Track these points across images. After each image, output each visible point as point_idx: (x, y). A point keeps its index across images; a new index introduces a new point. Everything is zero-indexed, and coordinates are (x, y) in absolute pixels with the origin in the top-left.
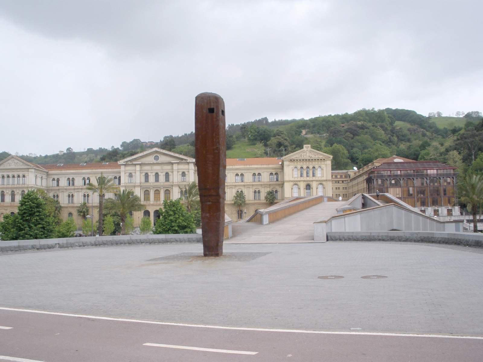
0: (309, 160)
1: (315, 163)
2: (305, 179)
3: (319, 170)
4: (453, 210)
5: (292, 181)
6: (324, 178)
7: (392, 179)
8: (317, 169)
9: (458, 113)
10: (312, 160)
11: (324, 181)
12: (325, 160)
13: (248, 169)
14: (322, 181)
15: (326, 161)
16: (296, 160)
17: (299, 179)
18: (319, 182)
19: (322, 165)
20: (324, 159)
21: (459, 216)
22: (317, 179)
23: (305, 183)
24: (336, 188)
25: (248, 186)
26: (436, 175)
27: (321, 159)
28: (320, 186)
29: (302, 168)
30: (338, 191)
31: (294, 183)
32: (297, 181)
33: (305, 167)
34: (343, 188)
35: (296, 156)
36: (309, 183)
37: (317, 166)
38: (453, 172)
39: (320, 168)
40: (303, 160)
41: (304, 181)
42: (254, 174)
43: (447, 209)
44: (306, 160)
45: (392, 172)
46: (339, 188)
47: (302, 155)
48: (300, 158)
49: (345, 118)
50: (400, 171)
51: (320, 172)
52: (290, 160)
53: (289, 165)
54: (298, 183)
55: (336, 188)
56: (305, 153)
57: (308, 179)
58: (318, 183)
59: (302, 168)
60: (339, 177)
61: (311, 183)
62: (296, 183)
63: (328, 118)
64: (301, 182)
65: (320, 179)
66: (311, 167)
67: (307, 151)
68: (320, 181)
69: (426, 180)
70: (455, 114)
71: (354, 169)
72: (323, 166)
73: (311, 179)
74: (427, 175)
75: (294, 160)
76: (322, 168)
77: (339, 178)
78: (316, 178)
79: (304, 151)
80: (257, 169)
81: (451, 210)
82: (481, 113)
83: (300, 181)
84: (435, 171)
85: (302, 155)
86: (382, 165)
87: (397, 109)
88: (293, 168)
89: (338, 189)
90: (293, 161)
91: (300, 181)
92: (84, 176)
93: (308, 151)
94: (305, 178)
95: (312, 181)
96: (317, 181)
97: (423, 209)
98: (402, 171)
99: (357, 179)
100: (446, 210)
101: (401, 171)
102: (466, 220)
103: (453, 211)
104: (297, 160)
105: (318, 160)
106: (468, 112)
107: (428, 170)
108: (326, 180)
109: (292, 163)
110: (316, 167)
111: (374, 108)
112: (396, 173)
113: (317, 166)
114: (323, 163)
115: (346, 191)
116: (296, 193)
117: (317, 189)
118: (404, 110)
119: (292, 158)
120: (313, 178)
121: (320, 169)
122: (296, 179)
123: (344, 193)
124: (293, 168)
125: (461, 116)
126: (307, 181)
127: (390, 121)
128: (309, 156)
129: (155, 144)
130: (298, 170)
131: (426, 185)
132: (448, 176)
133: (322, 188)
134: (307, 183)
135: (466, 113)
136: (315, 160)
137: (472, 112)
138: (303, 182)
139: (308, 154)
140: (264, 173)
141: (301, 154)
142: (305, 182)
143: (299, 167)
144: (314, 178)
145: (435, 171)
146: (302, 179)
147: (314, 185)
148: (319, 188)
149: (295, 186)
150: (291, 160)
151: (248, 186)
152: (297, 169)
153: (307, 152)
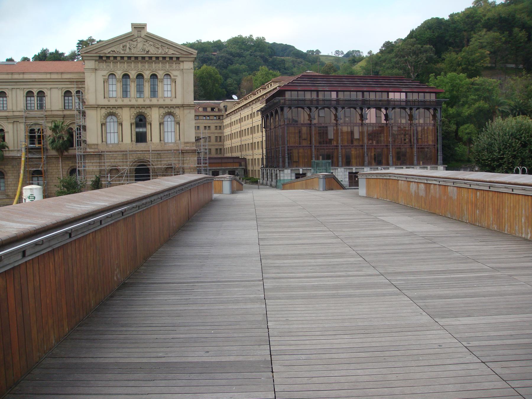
0: (143, 58)
2: (133, 102)
5: (103, 107)
6: (178, 101)
7: (319, 108)
8: (162, 80)
9: (337, 52)
10: (150, 58)
11: (178, 107)
12: (181, 59)
13: (17, 82)
14: (172, 106)
15: (183, 62)
16: (112, 59)
17: (120, 102)
18: (167, 110)
19: (173, 70)
20: (178, 58)
22: (161, 102)
23: (134, 112)
24: (205, 127)
25: (16, 120)
26: (404, 103)
27: (171, 58)
28: (169, 120)
29: (126, 76)
30: (207, 131)
31: (109, 110)
32: (114, 107)
33: (133, 74)
34: (216, 127)
35: (113, 49)
36: (143, 110)
38: (436, 98)
39: (168, 77)
40: (129, 58)
41: (132, 107)
42: (30, 94)
44: (136, 58)
45: (321, 94)
46: (209, 127)
47: (128, 46)
48: (123, 52)
49: (218, 45)
50: (404, 94)
52: (97, 58)
53: (96, 69)
54: (119, 111)
55: (205, 127)
56: (135, 43)
57: (141, 102)
58: (162, 111)
59: (126, 76)
60: (209, 109)
61: (147, 111)
62: (111, 111)
64: (124, 109)
65: (168, 102)
66: (147, 74)
67: (138, 37)
68: (167, 106)
69: (334, 113)
70: (334, 53)
71: (233, 99)
73: (148, 102)
74: (388, 101)
75: (108, 58)
76: (173, 77)
77: (209, 112)
78: (158, 101)
79: (131, 38)
80: (35, 81)
82: (362, 52)
83: (121, 107)
84: (403, 96)
85: (126, 46)
86: (298, 79)
87: (275, 43)
88: (107, 77)
89: (207, 128)
90: (105, 61)
92: (29, 87)
93: (141, 37)
94: (133, 99)
95: (150, 107)
96: (161, 107)
98: (408, 94)
99: (239, 113)
101: (363, 92)
104: (115, 58)
105: (164, 58)
106: (348, 51)
107: (390, 93)
108: (183, 106)
109: (103, 65)
110: (160, 74)
112: (327, 96)
114: (174, 66)
115: (209, 131)
116: (112, 134)
117: (162, 126)
118: (282, 44)
119: (103, 52)
122: (113, 102)
123: (216, 135)
125: (340, 56)
126: (138, 107)
128: (144, 50)
131: (335, 122)
132: (425, 105)
133: (173, 123)
134: (138, 110)
135: (345, 53)
136: (157, 58)
137: (353, 51)
139: (140, 46)
140: (53, 90)
141: (124, 44)
142: (133, 110)
143: (119, 74)
144: (154, 101)
145: (403, 96)
146: (126, 101)
147: (154, 116)
148: (166, 123)
149: (110, 117)
150: (101, 57)
151: (16, 120)
153: (139, 40)
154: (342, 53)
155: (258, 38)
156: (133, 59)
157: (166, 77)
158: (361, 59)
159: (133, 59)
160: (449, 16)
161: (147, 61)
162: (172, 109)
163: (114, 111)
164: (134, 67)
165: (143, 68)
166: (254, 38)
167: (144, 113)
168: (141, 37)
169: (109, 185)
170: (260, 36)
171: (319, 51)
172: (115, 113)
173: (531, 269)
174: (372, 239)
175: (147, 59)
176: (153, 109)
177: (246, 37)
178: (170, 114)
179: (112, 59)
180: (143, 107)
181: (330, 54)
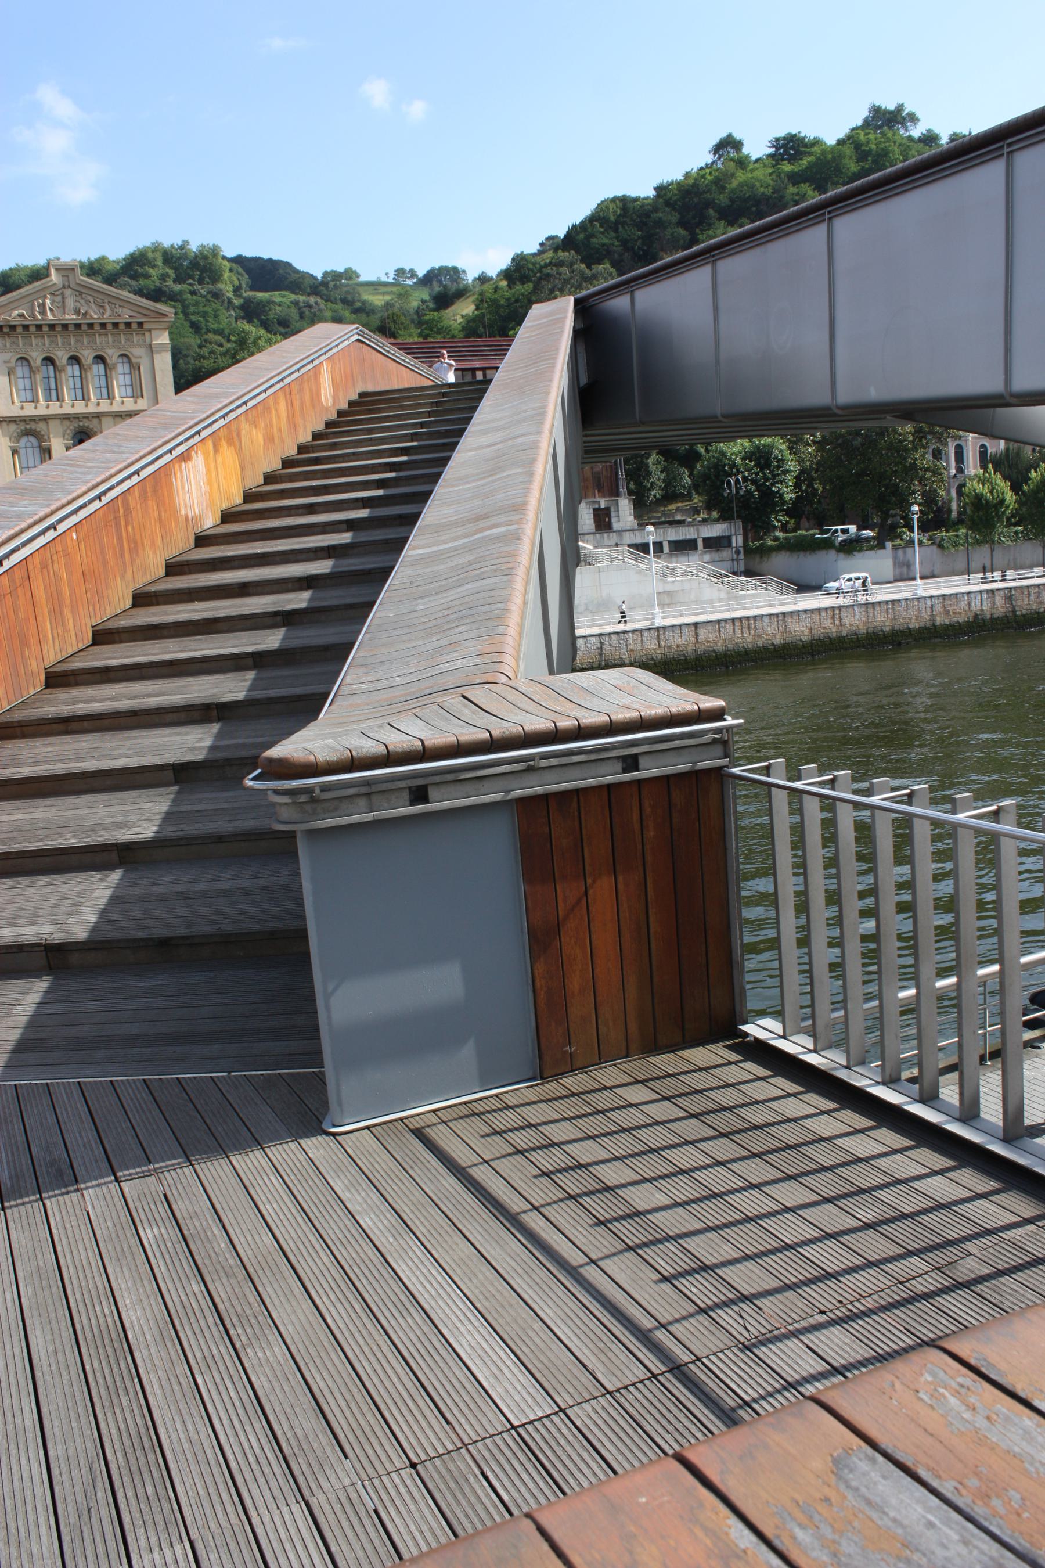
1: (104, 338)
2: (67, 409)
3: (122, 368)
4: (612, 509)
10: (91, 326)
12: (146, 326)
19: (135, 346)
20: (140, 324)
21: (633, 530)
27: (128, 325)
32: (33, 419)
37: (110, 351)
39: (25, 363)
41: (66, 417)
43: (594, 510)
51: (128, 377)
57: (80, 408)
63: (806, 146)
72: (138, 353)
73: (92, 409)
75: (13, 328)
76: (134, 360)
81: (607, 511)
88: (12, 364)
90: (8, 334)
91: (45, 420)
93: (69, 287)
97: (602, 506)
100: (591, 511)
102: (670, 542)
103: (613, 514)
106: (429, 269)
111: (902, 105)
113: (110, 351)
120: (48, 407)
121: (127, 366)
124: (12, 364)
126: (76, 417)
127: (237, 283)
129: (122, 268)
130: (32, 371)
133: (37, 450)
138: (58, 422)
142: (67, 423)
146: (55, 409)
149: (24, 440)
152: (30, 365)
154: (413, 273)
155: (202, 246)
156: (58, 329)
157: (19, 363)
158: (461, 293)
159: (58, 329)
160: (655, 189)
161: (85, 332)
162: (32, 423)
163: (33, 427)
164: (63, 344)
165: (79, 345)
166: (194, 247)
167: (88, 427)
168: (69, 287)
169: (413, 337)
170: (209, 241)
171: (355, 272)
172: (35, 430)
173: (1042, 938)
174: (453, 539)
175: (84, 328)
176: (52, 423)
177: (172, 246)
178: (28, 433)
179: (19, 329)
180: (87, 417)
181: (384, 279)
